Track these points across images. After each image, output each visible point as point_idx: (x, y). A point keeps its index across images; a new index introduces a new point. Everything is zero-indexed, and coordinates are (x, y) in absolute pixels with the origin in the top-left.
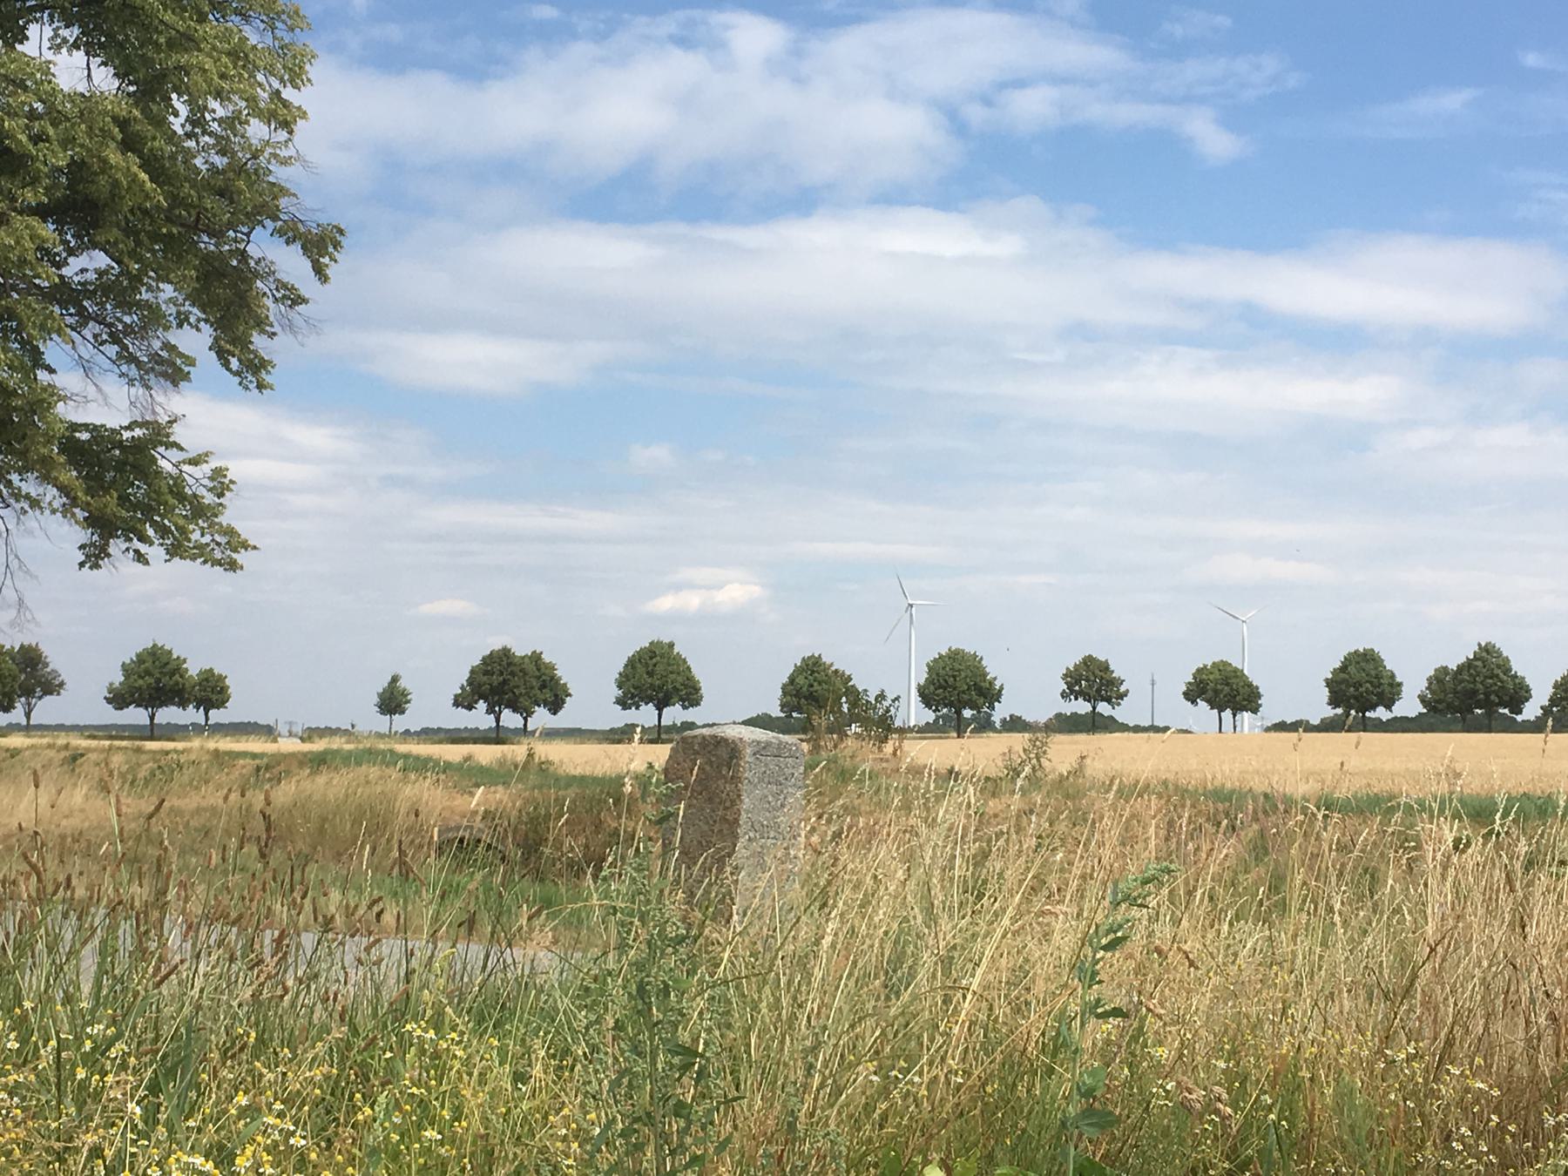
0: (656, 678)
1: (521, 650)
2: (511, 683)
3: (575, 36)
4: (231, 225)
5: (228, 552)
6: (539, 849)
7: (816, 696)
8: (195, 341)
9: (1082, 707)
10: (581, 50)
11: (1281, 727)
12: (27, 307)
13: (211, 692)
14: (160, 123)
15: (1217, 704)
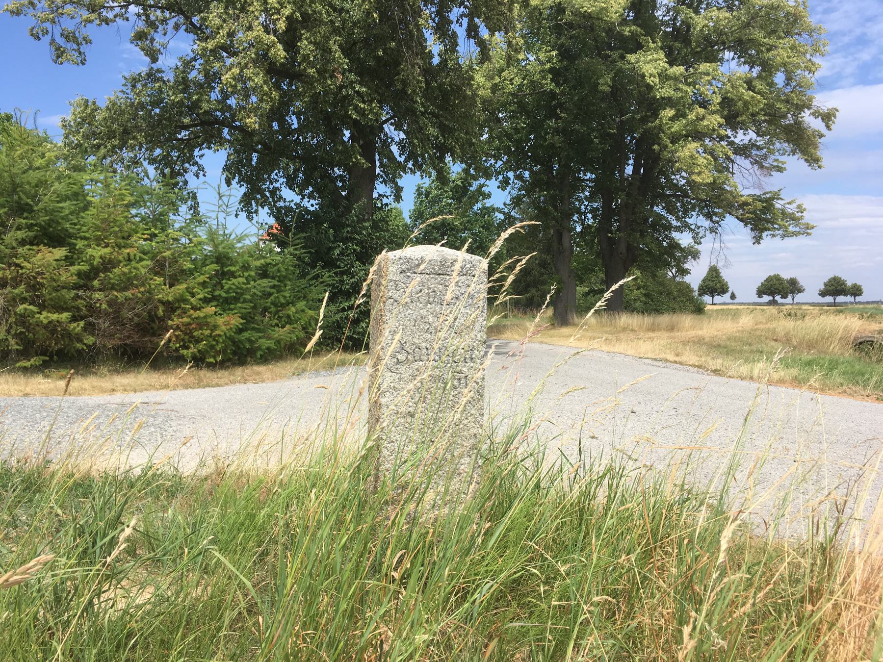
5: (807, 230)
13: (856, 291)
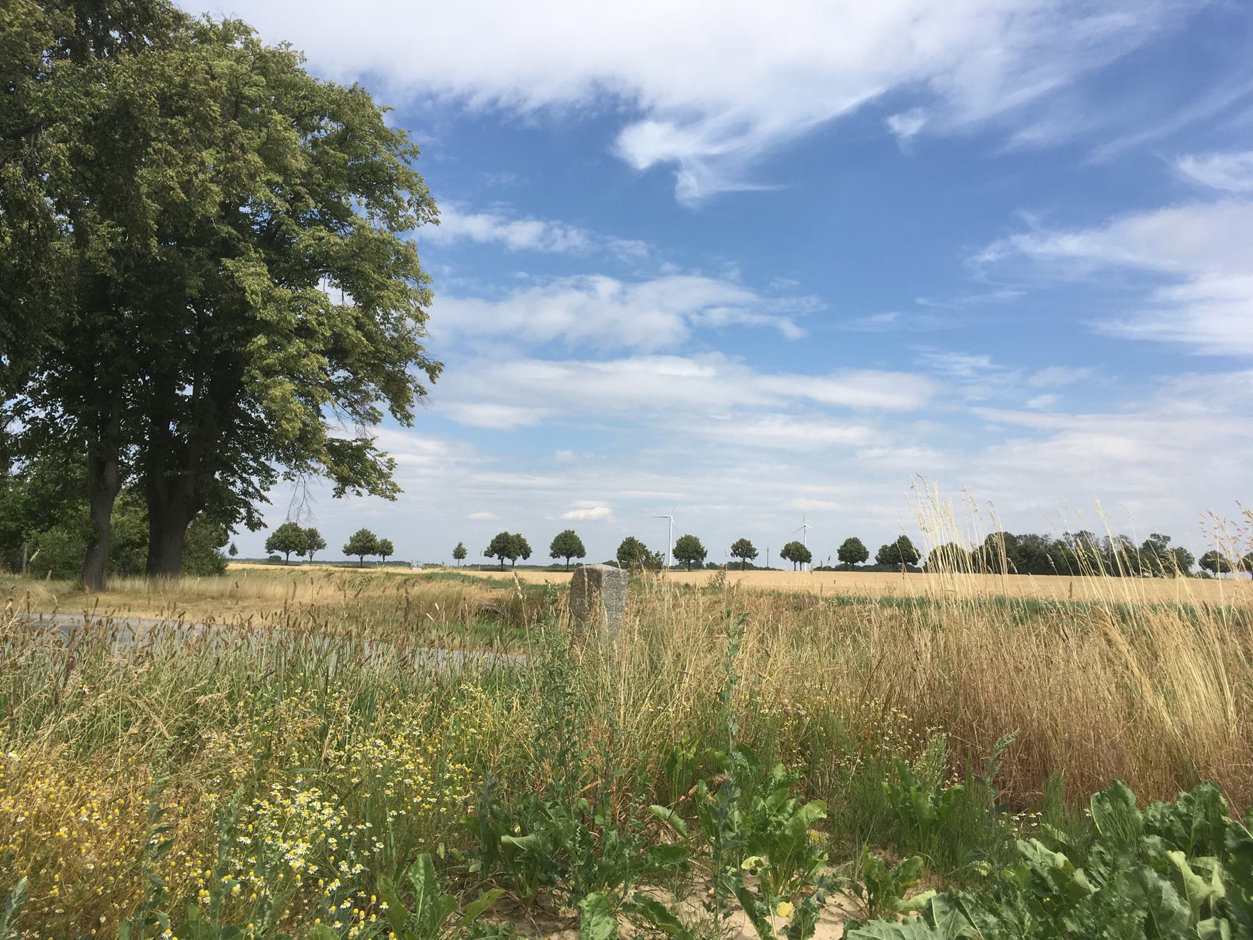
0: (567, 545)
1: (512, 533)
2: (508, 547)
3: (534, 285)
4: (399, 360)
5: (391, 492)
6: (509, 617)
7: (630, 552)
8: (383, 406)
9: (739, 559)
10: (537, 290)
11: (819, 569)
12: (318, 392)
13: (386, 549)
14: (372, 318)
15: (794, 559)
